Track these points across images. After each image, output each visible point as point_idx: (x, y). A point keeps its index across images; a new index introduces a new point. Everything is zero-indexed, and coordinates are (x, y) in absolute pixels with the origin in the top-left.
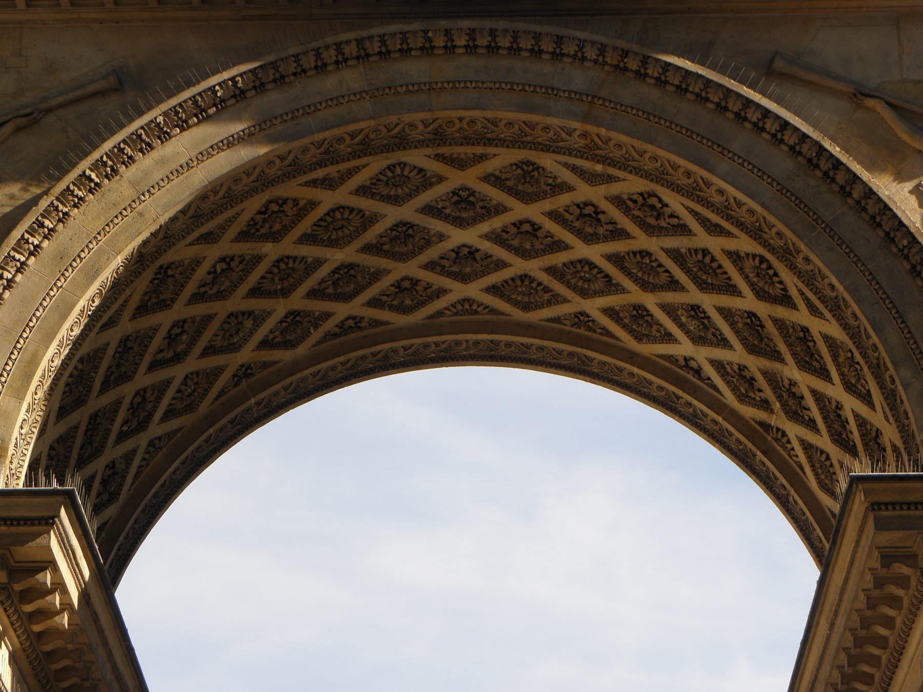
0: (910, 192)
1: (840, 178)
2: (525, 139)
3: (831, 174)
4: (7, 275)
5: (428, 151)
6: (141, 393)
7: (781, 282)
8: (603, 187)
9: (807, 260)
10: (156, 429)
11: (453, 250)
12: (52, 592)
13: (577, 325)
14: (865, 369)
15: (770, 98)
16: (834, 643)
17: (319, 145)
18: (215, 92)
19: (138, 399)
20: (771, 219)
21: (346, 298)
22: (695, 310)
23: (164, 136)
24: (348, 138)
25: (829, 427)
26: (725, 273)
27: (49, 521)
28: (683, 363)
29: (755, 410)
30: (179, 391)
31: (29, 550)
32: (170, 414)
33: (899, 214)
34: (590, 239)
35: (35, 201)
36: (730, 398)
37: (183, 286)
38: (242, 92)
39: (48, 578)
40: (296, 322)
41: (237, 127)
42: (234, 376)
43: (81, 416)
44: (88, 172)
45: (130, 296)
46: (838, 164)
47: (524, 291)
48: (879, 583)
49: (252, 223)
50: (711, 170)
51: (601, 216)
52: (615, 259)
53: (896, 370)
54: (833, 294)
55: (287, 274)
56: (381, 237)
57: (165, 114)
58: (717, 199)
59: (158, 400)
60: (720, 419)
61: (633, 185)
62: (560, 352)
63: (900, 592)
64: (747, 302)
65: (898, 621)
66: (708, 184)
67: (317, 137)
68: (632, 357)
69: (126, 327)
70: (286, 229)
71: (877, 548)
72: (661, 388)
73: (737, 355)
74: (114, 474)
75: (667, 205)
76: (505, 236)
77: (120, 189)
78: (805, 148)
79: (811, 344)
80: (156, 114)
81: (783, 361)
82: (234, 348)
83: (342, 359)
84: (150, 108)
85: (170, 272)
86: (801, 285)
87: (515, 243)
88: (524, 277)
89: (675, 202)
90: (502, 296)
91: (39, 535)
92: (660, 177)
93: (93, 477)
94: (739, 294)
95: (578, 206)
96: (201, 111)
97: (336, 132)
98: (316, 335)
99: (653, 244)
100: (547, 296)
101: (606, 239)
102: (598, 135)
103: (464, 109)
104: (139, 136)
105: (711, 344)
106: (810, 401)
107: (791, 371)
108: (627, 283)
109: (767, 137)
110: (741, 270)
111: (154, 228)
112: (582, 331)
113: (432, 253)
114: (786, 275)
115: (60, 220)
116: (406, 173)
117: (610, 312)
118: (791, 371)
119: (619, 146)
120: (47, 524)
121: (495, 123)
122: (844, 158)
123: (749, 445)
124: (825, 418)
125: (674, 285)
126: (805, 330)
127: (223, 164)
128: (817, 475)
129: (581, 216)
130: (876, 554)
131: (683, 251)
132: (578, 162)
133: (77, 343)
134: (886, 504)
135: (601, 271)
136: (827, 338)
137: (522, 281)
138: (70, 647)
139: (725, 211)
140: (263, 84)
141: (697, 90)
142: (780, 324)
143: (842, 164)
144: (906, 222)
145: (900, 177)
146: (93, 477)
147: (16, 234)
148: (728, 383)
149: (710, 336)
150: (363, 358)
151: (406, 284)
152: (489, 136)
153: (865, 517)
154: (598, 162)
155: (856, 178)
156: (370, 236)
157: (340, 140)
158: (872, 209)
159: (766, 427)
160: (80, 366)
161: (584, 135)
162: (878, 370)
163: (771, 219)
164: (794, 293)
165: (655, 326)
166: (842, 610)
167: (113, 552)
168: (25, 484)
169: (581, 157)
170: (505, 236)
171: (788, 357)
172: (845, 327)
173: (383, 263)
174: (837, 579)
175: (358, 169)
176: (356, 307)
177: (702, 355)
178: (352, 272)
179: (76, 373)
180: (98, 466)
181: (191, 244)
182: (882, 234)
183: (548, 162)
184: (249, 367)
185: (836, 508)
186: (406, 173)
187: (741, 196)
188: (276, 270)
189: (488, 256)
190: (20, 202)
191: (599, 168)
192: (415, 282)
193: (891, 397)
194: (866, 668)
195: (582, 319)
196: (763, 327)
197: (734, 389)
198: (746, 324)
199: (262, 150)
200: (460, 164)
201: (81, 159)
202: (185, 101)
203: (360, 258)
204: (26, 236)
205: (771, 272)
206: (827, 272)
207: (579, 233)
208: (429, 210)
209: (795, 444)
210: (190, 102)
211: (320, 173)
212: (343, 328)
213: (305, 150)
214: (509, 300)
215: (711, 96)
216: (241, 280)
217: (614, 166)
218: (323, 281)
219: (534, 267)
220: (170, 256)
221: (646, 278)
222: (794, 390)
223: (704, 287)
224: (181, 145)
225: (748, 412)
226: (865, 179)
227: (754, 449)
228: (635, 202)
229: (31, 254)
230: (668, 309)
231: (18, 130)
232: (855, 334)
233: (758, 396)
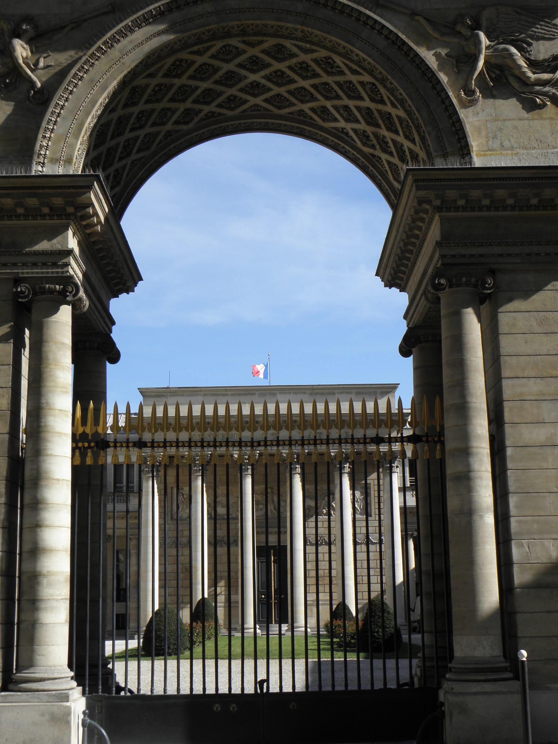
0: (433, 55)
1: (405, 49)
2: (278, 33)
3: (401, 47)
4: (70, 88)
5: (239, 39)
6: (127, 141)
7: (380, 94)
8: (310, 55)
9: (391, 83)
11: (250, 83)
12: (93, 216)
14: (413, 128)
15: (377, 15)
16: (398, 238)
17: (195, 35)
18: (152, 12)
19: (126, 144)
20: (377, 66)
21: (208, 103)
22: (346, 108)
23: (132, 31)
24: (206, 32)
25: (398, 154)
26: (358, 91)
27: (90, 187)
28: (341, 130)
29: (369, 149)
30: (143, 141)
31: (82, 199)
32: (139, 150)
33: (428, 63)
34: (304, 78)
35: (80, 58)
36: (359, 144)
37: (142, 96)
38: (163, 12)
39: (91, 211)
40: (188, 114)
41: (162, 27)
42: (164, 136)
43: (103, 149)
44: (101, 46)
45: (120, 99)
46: (404, 43)
47: (279, 101)
48: (417, 212)
49: (169, 70)
50: (353, 45)
51: (309, 68)
52: (314, 86)
53: (425, 127)
54: (401, 97)
55: (184, 93)
56: (221, 77)
57: (132, 21)
58: (355, 58)
59: (134, 144)
60: (355, 153)
61: (322, 53)
62: (293, 127)
63: (425, 216)
64: (367, 103)
65: (424, 227)
66: (352, 52)
67: (194, 32)
68: (321, 128)
69: (120, 112)
70: (183, 73)
71: (417, 198)
72: (332, 141)
73: (362, 126)
74: (118, 174)
75: (335, 62)
76: (271, 77)
77: (114, 53)
78: (391, 36)
79: (392, 120)
80: (128, 21)
81: (380, 128)
82: (164, 124)
83: (207, 129)
84: (125, 19)
85: (137, 90)
86: (388, 94)
87: (275, 80)
88: (278, 95)
89: (338, 60)
91: (86, 193)
92: (331, 49)
93: (109, 175)
95: (300, 63)
96: (146, 20)
97: (202, 30)
98: (196, 119)
99: (330, 80)
100: (287, 103)
101: (311, 78)
102: (308, 31)
103: (254, 20)
104: (122, 31)
105: (352, 122)
106: (391, 144)
107: (384, 132)
108: (319, 97)
109: (375, 31)
110: (365, 90)
111: (129, 69)
112: (301, 118)
113: (242, 85)
114: (382, 90)
115: (91, 66)
116: (231, 49)
117: (313, 109)
118: (384, 132)
119: (316, 36)
120: (89, 188)
121: (266, 26)
122: (407, 40)
123: (367, 163)
124: (397, 151)
125: (338, 97)
126: (390, 114)
127: (156, 42)
128: (393, 174)
129: (301, 68)
130: (416, 200)
131: (342, 82)
132: (300, 44)
133: (100, 117)
134: (420, 180)
135: (309, 92)
136: (398, 117)
137: (278, 97)
138: (102, 239)
139: (358, 63)
140: (171, 9)
141: (348, 12)
142: (379, 111)
143: (406, 43)
144: (431, 67)
145: (429, 49)
146: (109, 175)
147: (73, 71)
148: (359, 138)
149: (352, 118)
150: (215, 129)
151: (232, 98)
152: (264, 32)
153: (412, 186)
154: (308, 43)
155: (411, 49)
156: (217, 76)
157: (203, 33)
158: (417, 62)
159: (373, 156)
160: (102, 128)
161: (302, 31)
162: (418, 128)
163: (377, 66)
164: (385, 98)
165: (330, 115)
166: (402, 225)
167: (119, 205)
168: (82, 172)
169: (301, 41)
170: (271, 77)
171: (383, 126)
172: (406, 111)
173: (222, 88)
174: (400, 212)
175: (211, 47)
176: (212, 107)
177: (349, 127)
178: (210, 92)
179: (100, 131)
180: (111, 170)
181: (144, 78)
182: (421, 71)
183: (288, 44)
184: (170, 132)
186: (231, 49)
187: (365, 57)
188: (179, 91)
189: (264, 86)
190: (75, 59)
191: (308, 46)
192: (235, 97)
193: (423, 139)
194: (410, 248)
195: (301, 112)
196: (373, 113)
197: (361, 141)
198: (366, 113)
199: (172, 37)
200: (252, 45)
201: (98, 40)
202: (140, 16)
203: (212, 86)
204: (77, 72)
205: (376, 90)
206: (399, 88)
207: (300, 75)
208: (240, 65)
209: (385, 162)
210: (142, 17)
211: (195, 48)
212: (207, 117)
213: (189, 37)
214: (273, 105)
215: (353, 14)
217: (314, 45)
218: (198, 96)
219: (282, 90)
220: (136, 83)
221: (327, 94)
222: (384, 140)
223: (350, 97)
224: (139, 34)
225: (366, 150)
226: (415, 49)
227: (368, 165)
228: (323, 61)
229: (80, 80)
230: (335, 107)
231: (72, 29)
232: (409, 113)
233: (370, 143)
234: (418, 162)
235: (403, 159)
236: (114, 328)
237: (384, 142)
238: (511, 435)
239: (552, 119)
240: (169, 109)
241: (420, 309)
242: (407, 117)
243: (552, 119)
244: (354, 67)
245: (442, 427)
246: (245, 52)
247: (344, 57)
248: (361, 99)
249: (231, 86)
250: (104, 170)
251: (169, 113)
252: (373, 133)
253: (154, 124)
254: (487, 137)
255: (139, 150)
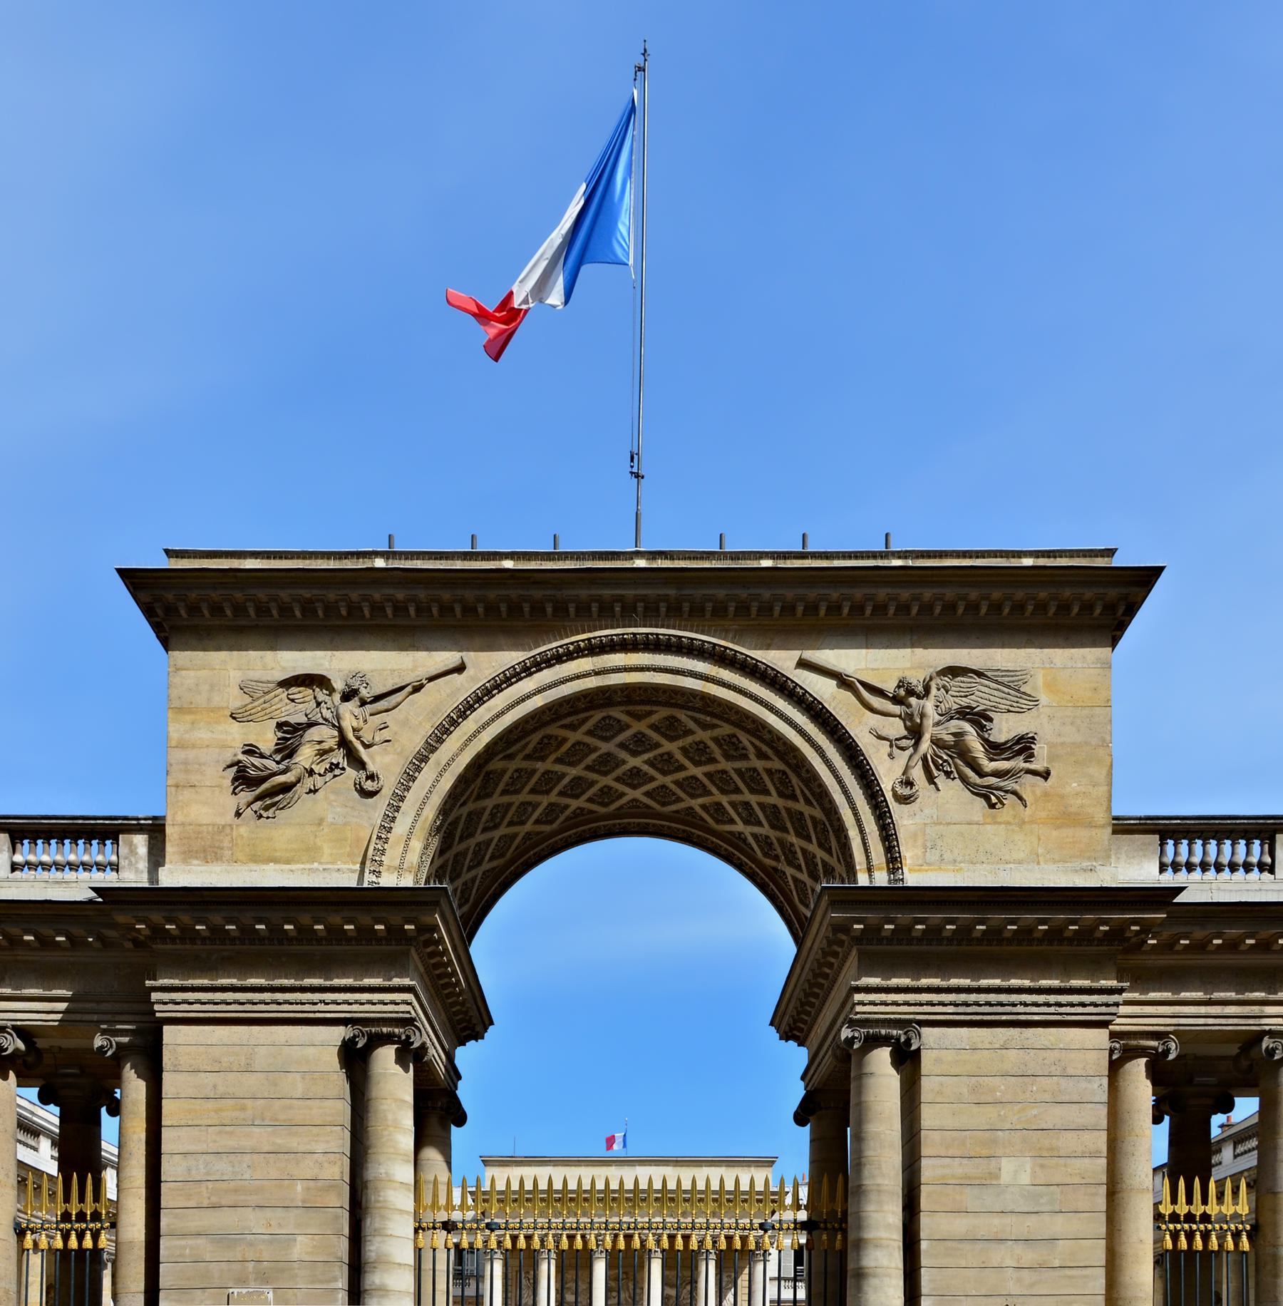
5: (623, 708)
6: (478, 844)
10: (486, 866)
13: (688, 815)
21: (577, 797)
22: (747, 805)
32: (492, 858)
43: (450, 855)
55: (550, 780)
63: (839, 950)
64: (774, 799)
73: (765, 830)
81: (788, 832)
82: (523, 823)
90: (652, 798)
94: (770, 794)
98: (562, 818)
101: (705, 763)
105: (753, 824)
107: (793, 839)
108: (714, 790)
110: (772, 780)
114: (795, 780)
118: (793, 839)
124: (806, 864)
126: (801, 813)
136: (812, 818)
142: (788, 810)
159: (775, 869)
164: (798, 792)
171: (791, 830)
172: (823, 809)
173: (594, 776)
174: (808, 943)
175: (587, 719)
177: (747, 830)
180: (459, 882)
183: (682, 715)
185: (809, 914)
189: (646, 774)
192: (610, 788)
194: (816, 990)
200: (639, 717)
203: (701, 777)
211: (567, 721)
214: (655, 800)
216: (526, 783)
219: (668, 780)
223: (752, 791)
234: (834, 878)
235: (816, 878)
236: (460, 1083)
237: (791, 851)
238: (927, 1225)
239: (1008, 823)
240: (530, 803)
241: (823, 1069)
242: (824, 819)
243: (1008, 823)
244: (765, 748)
245: (845, 1213)
246: (628, 727)
247: (754, 735)
248: (767, 793)
249: (605, 774)
250: (452, 881)
251: (530, 809)
252: (778, 840)
253: (511, 824)
254: (925, 847)
255: (492, 858)
